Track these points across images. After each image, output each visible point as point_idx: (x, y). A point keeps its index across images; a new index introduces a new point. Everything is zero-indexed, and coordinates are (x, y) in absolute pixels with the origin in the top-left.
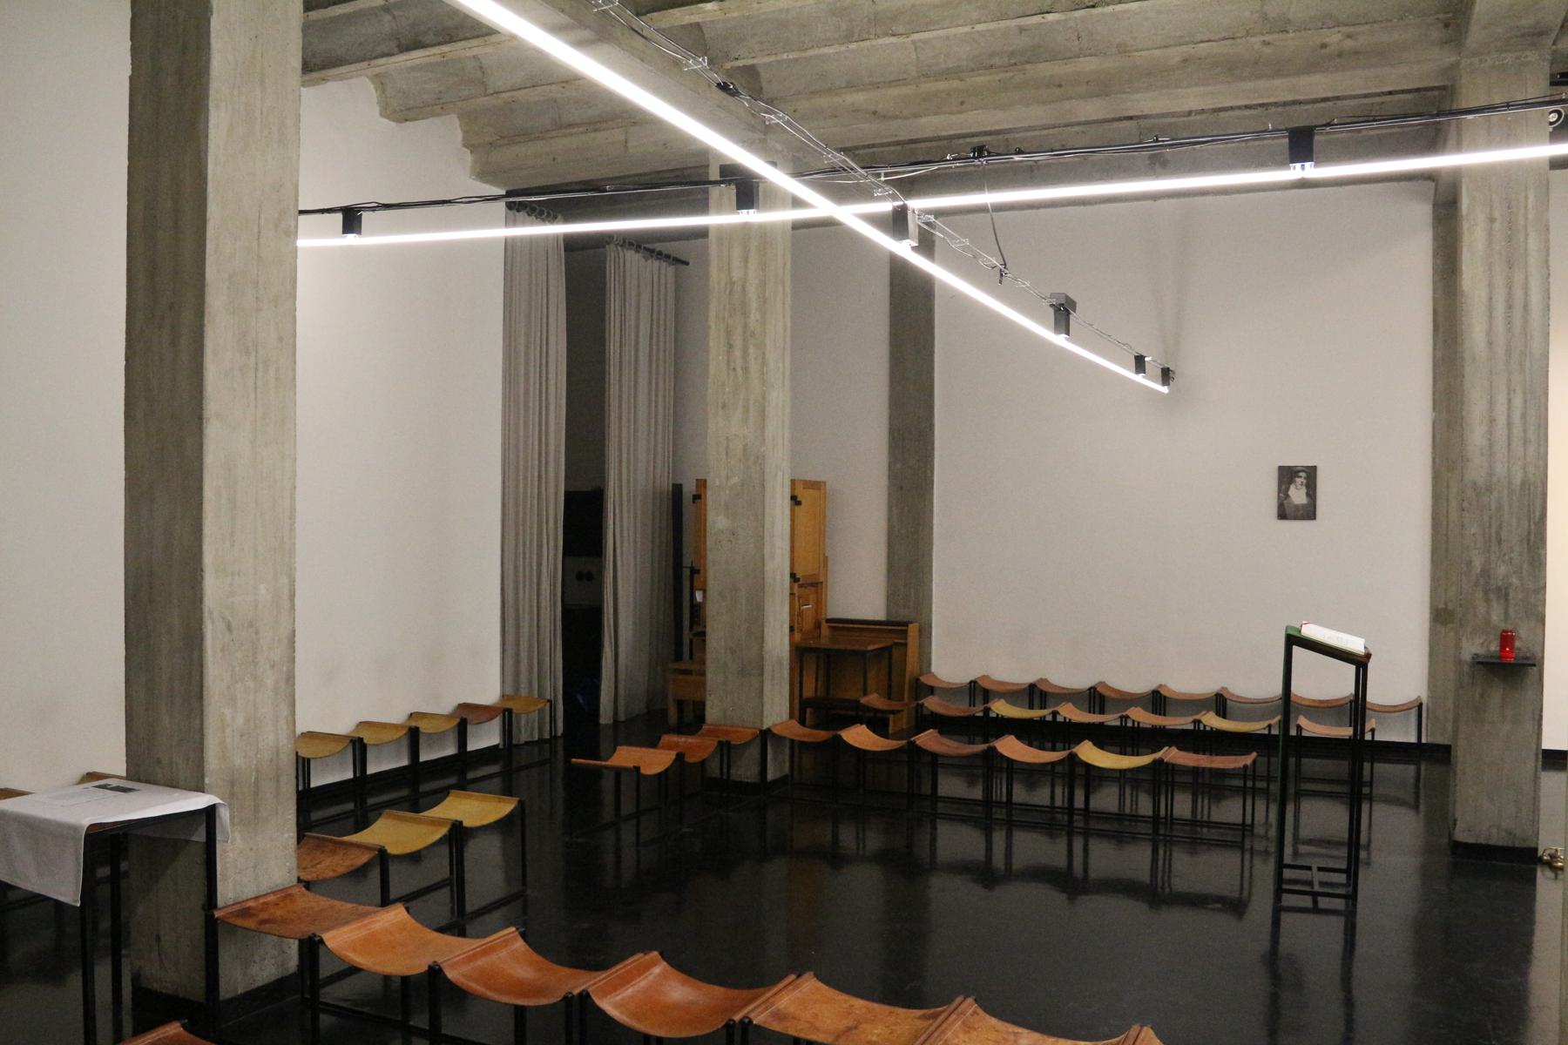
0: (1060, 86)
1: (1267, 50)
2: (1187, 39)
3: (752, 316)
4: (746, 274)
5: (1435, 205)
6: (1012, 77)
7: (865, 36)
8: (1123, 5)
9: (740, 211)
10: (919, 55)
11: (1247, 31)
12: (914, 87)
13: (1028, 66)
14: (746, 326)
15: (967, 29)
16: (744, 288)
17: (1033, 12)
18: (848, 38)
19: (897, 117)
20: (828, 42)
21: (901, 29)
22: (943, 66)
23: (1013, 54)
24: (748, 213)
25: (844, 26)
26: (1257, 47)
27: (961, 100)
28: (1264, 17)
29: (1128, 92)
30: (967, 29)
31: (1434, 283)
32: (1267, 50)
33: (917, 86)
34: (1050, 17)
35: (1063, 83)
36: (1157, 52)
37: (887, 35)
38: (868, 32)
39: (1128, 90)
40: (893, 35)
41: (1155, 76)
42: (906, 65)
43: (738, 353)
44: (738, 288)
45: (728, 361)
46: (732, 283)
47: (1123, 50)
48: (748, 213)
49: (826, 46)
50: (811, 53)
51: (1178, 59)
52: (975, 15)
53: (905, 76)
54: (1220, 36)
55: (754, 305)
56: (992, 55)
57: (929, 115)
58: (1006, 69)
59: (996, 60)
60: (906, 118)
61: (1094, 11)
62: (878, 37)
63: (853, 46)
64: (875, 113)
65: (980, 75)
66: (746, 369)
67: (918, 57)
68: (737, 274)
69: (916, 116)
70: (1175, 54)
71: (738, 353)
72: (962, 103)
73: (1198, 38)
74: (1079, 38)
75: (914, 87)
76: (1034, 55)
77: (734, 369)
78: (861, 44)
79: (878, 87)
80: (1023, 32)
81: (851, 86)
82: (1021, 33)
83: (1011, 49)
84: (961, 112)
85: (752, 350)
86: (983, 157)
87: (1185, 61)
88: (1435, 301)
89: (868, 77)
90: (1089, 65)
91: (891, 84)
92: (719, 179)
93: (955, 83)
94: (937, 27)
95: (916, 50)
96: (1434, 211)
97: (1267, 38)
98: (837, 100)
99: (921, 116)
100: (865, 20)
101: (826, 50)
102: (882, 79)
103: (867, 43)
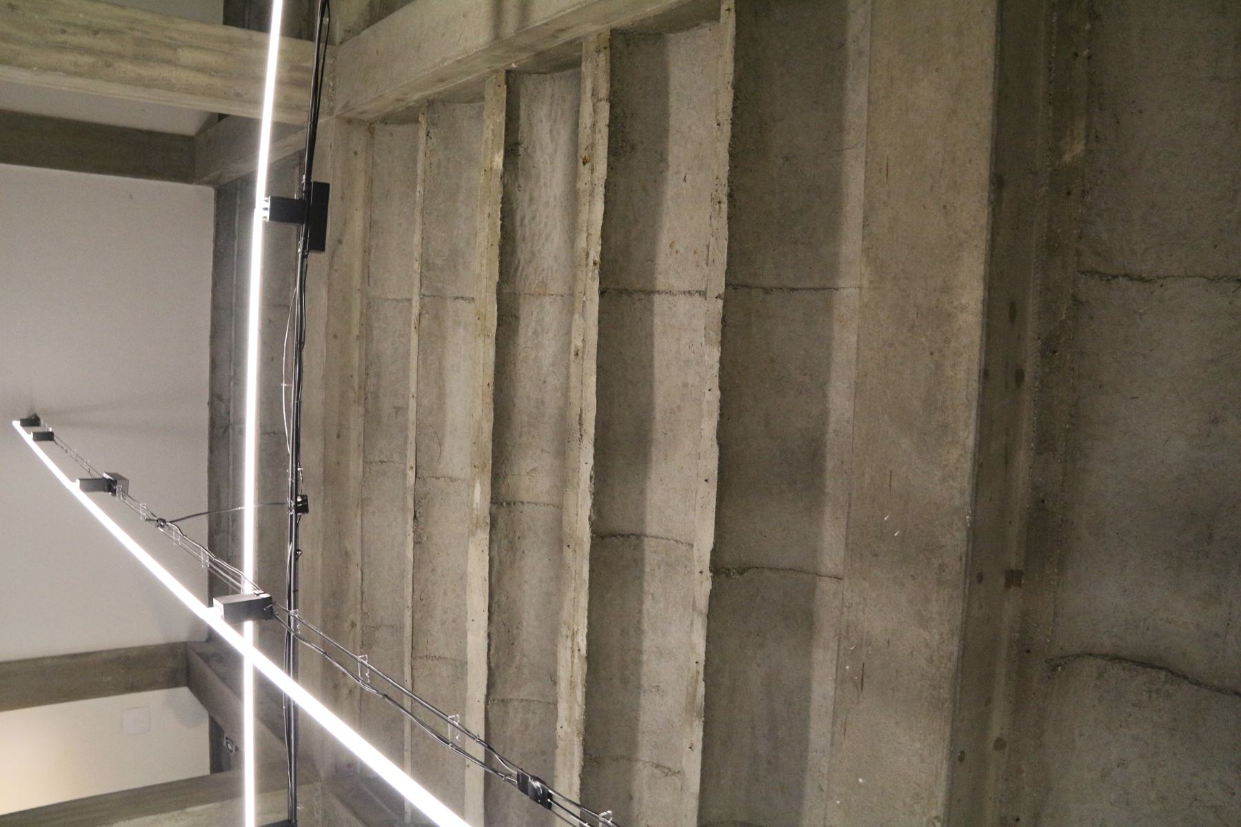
0: (338, 436)
1: (347, 626)
2: (366, 560)
3: (130, 67)
4: (185, 67)
5: (185, 644)
6: (352, 387)
7: (425, 282)
8: (412, 545)
9: (269, 199)
10: (389, 302)
11: (367, 613)
12: (359, 287)
13: (362, 410)
14: (121, 56)
15: (413, 389)
16: (169, 62)
17: (419, 460)
18: (426, 265)
19: (331, 267)
20: (425, 241)
21: (424, 323)
22: (376, 324)
23: (376, 396)
24: (266, 209)
25: (439, 261)
26: (352, 617)
27: (339, 335)
28: (377, 628)
29: (324, 503)
30: (413, 389)
31: (116, 650)
32: (347, 626)
33: (359, 290)
34: (411, 474)
35: (341, 439)
36: (359, 531)
37: (422, 308)
38: (427, 288)
39: (326, 502)
40: (420, 314)
41: (336, 531)
42: (383, 285)
43: (86, 40)
44: (168, 54)
45: (76, 25)
46: (174, 47)
47: (363, 503)
48: (266, 209)
49: (423, 238)
50: (418, 218)
51: (349, 548)
52: (426, 402)
53: (371, 284)
54: (365, 590)
55: (145, 71)
56: (378, 376)
57: (329, 300)
58: (362, 388)
59: (372, 380)
60: (329, 275)
61: (411, 516)
62: (421, 299)
63: (416, 266)
64: (340, 242)
65: (360, 359)
66: (62, 47)
67: (388, 300)
68: (186, 55)
69: (330, 286)
70: (353, 546)
71: (86, 40)
72: (335, 337)
73: (366, 571)
74: (382, 462)
75: (359, 287)
76: (372, 418)
77: (64, 32)
78: (418, 277)
79: (365, 252)
80: (395, 410)
81: (371, 226)
82: (394, 407)
83: (381, 395)
84: (327, 334)
85: (86, 60)
86: (296, 513)
87: (347, 553)
88: (99, 653)
89: (377, 245)
90: (355, 466)
91: (366, 266)
92: (312, 180)
93: (356, 331)
94: (420, 363)
95: (395, 300)
96: (183, 643)
97: (358, 627)
98: (359, 202)
99: (329, 292)
100: (440, 285)
101: (417, 238)
102: (372, 258)
103: (417, 283)
